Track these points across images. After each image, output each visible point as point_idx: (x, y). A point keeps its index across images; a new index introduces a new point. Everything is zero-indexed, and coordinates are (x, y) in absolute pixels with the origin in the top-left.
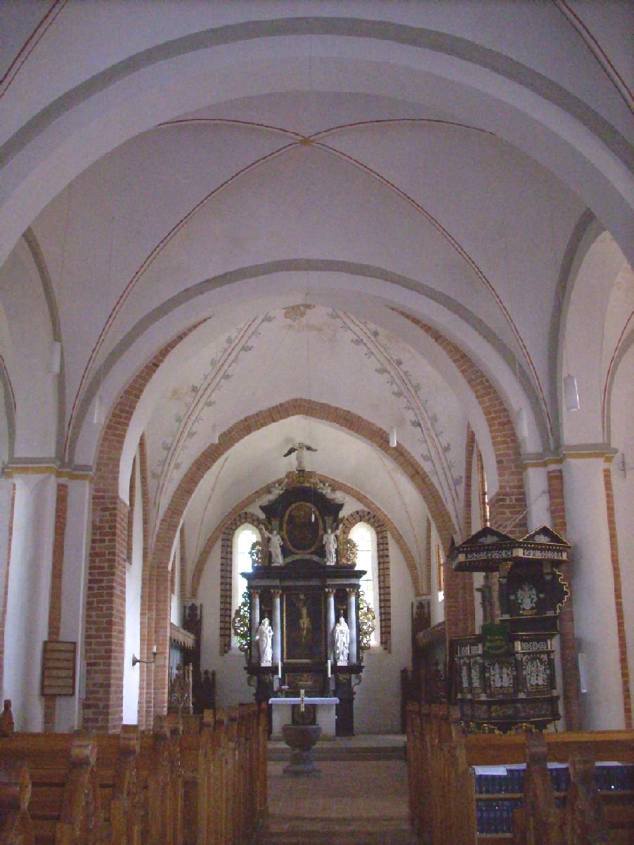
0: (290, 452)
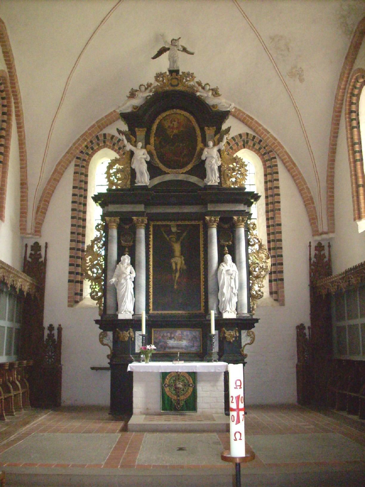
0: (162, 51)
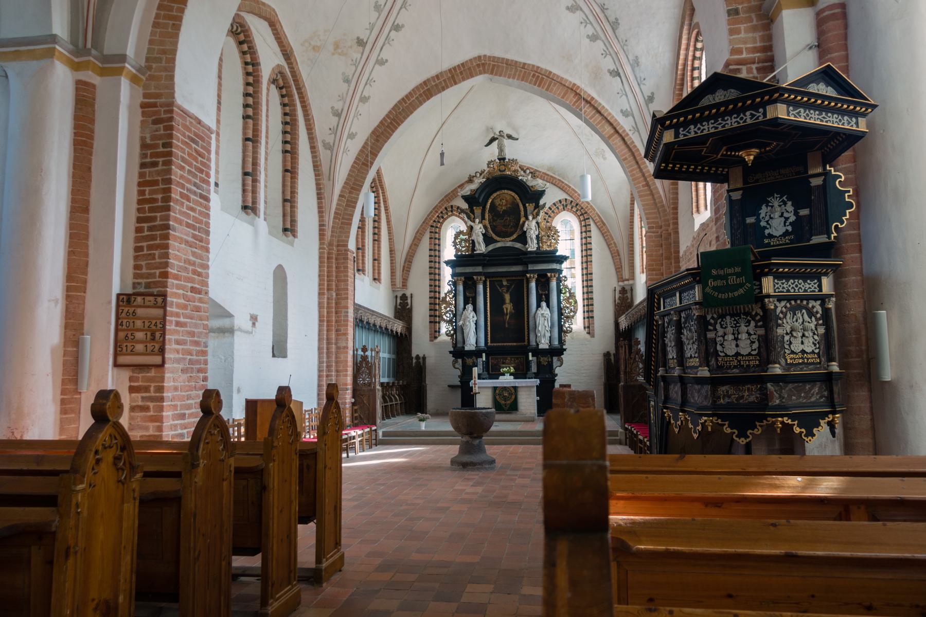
0: (493, 140)
